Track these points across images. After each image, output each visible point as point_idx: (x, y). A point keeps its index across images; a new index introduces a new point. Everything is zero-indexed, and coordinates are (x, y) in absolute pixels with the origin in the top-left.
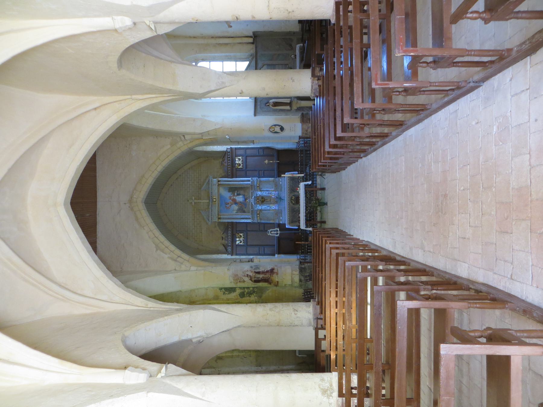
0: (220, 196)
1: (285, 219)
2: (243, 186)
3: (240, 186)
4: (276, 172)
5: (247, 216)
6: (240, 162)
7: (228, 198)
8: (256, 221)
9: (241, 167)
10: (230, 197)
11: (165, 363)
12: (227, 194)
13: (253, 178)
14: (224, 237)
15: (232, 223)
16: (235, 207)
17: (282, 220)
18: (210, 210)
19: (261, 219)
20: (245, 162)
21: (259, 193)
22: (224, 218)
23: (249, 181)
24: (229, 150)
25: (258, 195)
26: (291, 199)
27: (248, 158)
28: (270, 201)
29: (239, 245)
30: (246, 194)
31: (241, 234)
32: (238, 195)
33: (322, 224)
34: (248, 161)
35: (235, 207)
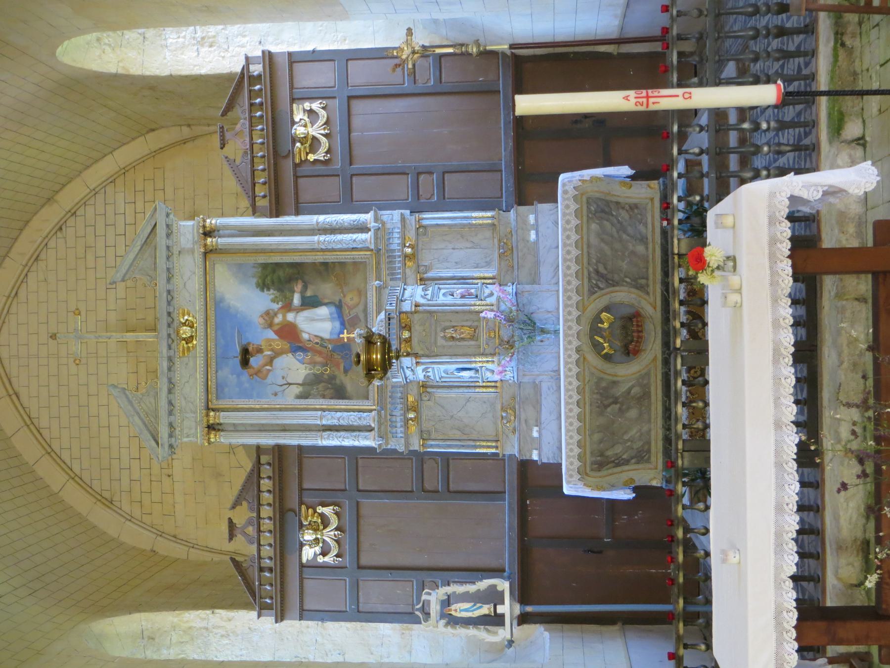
0: (218, 313)
1: (557, 436)
2: (330, 258)
3: (319, 258)
4: (507, 180)
5: (352, 419)
6: (316, 131)
7: (257, 320)
8: (398, 444)
9: (320, 155)
10: (269, 316)
11: (543, 464)
12: (250, 302)
13: (386, 215)
14: (239, 521)
15: (280, 451)
16: (294, 368)
17: (538, 444)
18: (163, 386)
19: (424, 436)
20: (344, 127)
21: (415, 294)
22: (236, 428)
23: (362, 228)
24: (256, 69)
25: (407, 307)
26: (595, 329)
27: (359, 107)
28: (474, 337)
29: (313, 566)
30: (350, 299)
31: (328, 511)
32: (310, 303)
33: (830, 239)
34: (356, 122)
35: (294, 368)
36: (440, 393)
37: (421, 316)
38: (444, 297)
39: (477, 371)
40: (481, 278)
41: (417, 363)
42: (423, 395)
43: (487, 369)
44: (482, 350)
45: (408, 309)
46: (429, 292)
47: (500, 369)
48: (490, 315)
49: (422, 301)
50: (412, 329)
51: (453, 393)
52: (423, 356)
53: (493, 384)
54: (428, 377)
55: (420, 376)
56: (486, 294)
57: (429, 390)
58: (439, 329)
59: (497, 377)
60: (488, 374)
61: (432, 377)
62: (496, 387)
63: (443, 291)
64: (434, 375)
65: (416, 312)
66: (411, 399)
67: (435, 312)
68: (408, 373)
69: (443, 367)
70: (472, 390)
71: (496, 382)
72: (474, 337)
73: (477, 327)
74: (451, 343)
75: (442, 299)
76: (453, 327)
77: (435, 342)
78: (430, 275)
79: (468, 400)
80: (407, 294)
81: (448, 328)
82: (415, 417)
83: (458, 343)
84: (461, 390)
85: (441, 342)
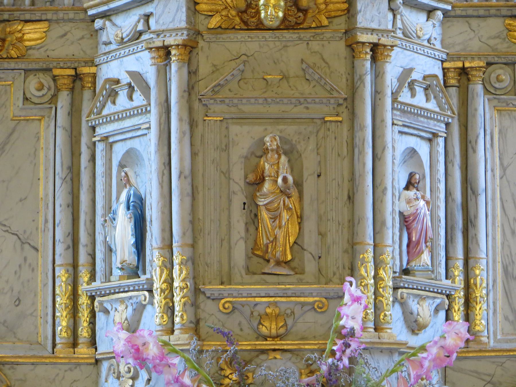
28: (261, 258)
36: (50, 138)
37: (340, 66)
38: (404, 150)
39: (135, 271)
40: (468, 287)
41: (165, 51)
42: (46, 80)
43: (140, 309)
44: (213, 288)
45: (363, 20)
46: (420, 99)
47: (152, 350)
48: (352, 315)
49: (392, 70)
50: (287, 35)
51: (50, 188)
52: (192, 73)
53: (84, 332)
54: (113, 95)
55: (114, 69)
56: (413, 305)
57: (64, 100)
58: (290, 130)
59: (112, 337)
60: (121, 313)
61: (109, 109)
62: (74, 344)
63: (423, 149)
64: (119, 117)
65: (353, 47)
66: (33, 33)
67: (353, 114)
68: (127, 23)
69: (148, 147)
70: (62, 256)
71: (93, 343)
72: (261, 258)
73: (299, 271)
74: (238, 174)
75: (397, 144)
76: (299, 185)
77: (242, 119)
78: (482, 105)
79: (25, 242)
80: (415, 19)
81: (295, 166)
82: (87, 12)
83: (238, 200)
84: (62, 216)
85: (244, 137)
